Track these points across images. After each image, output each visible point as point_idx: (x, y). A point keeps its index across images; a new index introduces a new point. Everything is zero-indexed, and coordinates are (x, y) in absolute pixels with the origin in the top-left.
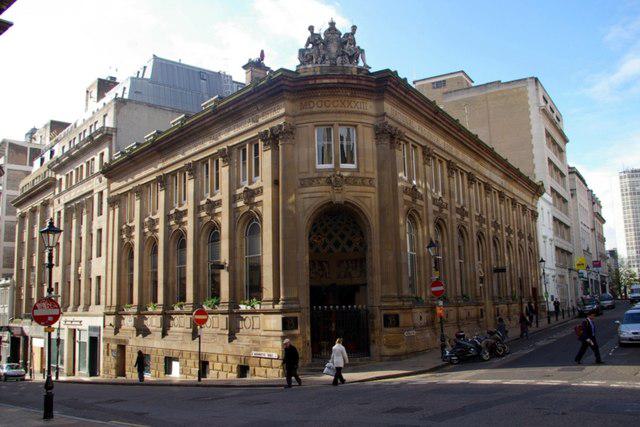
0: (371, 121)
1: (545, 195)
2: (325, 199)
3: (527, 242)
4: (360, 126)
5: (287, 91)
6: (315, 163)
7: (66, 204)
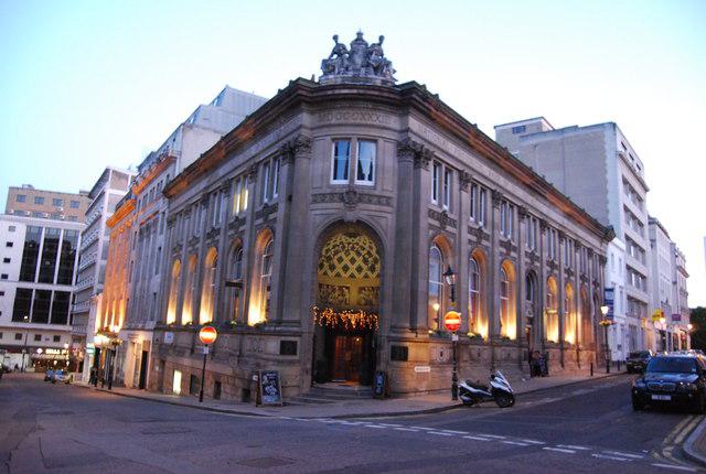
0: (394, 136)
1: (616, 240)
2: (335, 216)
3: (592, 286)
4: (381, 141)
5: (306, 102)
6: (329, 176)
7: (141, 224)
